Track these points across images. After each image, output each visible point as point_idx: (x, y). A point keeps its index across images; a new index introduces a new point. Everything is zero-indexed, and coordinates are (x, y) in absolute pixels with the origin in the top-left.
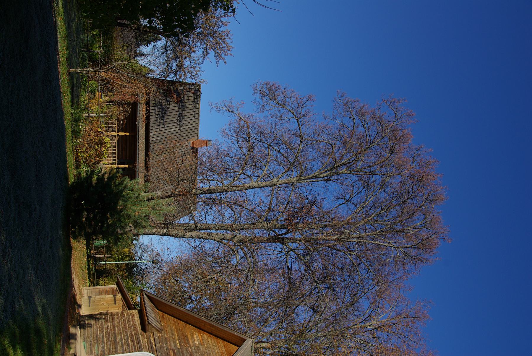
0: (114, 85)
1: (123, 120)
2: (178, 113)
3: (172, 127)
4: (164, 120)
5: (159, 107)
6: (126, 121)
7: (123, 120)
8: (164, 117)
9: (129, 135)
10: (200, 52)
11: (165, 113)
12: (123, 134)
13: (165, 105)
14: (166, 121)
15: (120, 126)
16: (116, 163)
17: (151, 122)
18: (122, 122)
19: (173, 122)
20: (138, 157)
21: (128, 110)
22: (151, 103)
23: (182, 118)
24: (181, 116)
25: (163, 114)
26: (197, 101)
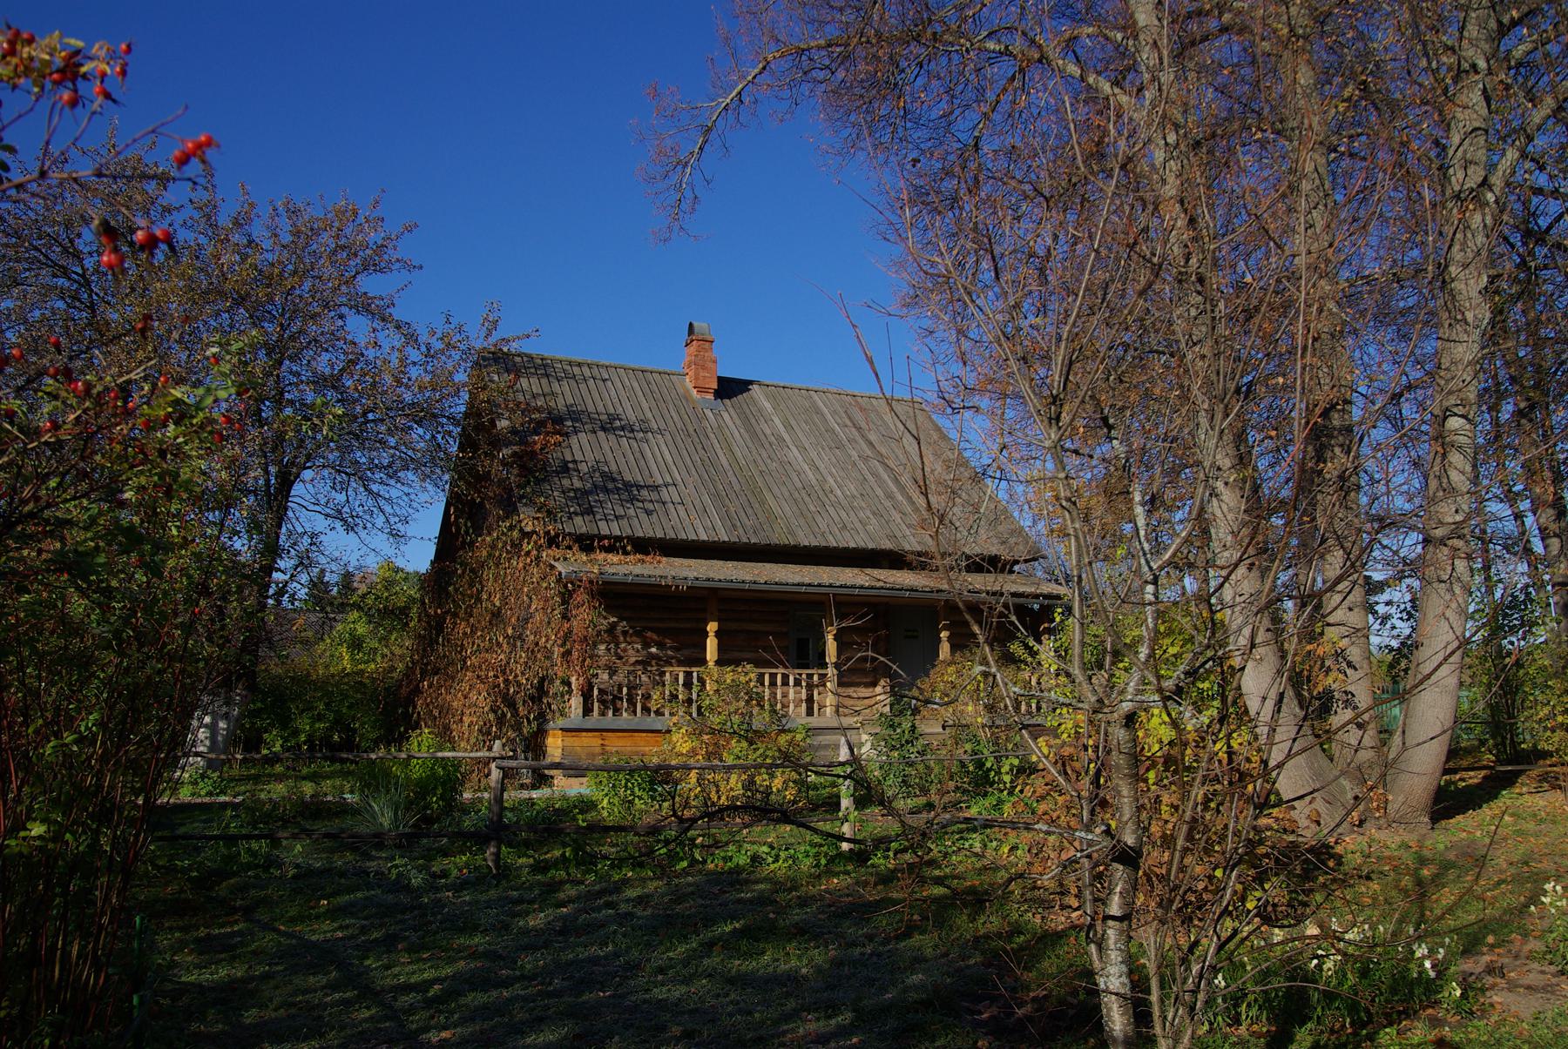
0: (516, 676)
1: (646, 645)
2: (601, 434)
3: (660, 459)
4: (639, 487)
5: (596, 501)
6: (649, 634)
7: (646, 645)
8: (628, 486)
9: (719, 621)
10: (358, 327)
11: (614, 480)
12: (711, 645)
13: (581, 478)
14: (640, 479)
15: (666, 655)
16: (821, 671)
17: (660, 535)
18: (654, 650)
19: (638, 455)
20: (810, 585)
21: (605, 622)
22: (584, 530)
23: (617, 423)
24: (609, 425)
25: (612, 486)
26: (545, 366)
